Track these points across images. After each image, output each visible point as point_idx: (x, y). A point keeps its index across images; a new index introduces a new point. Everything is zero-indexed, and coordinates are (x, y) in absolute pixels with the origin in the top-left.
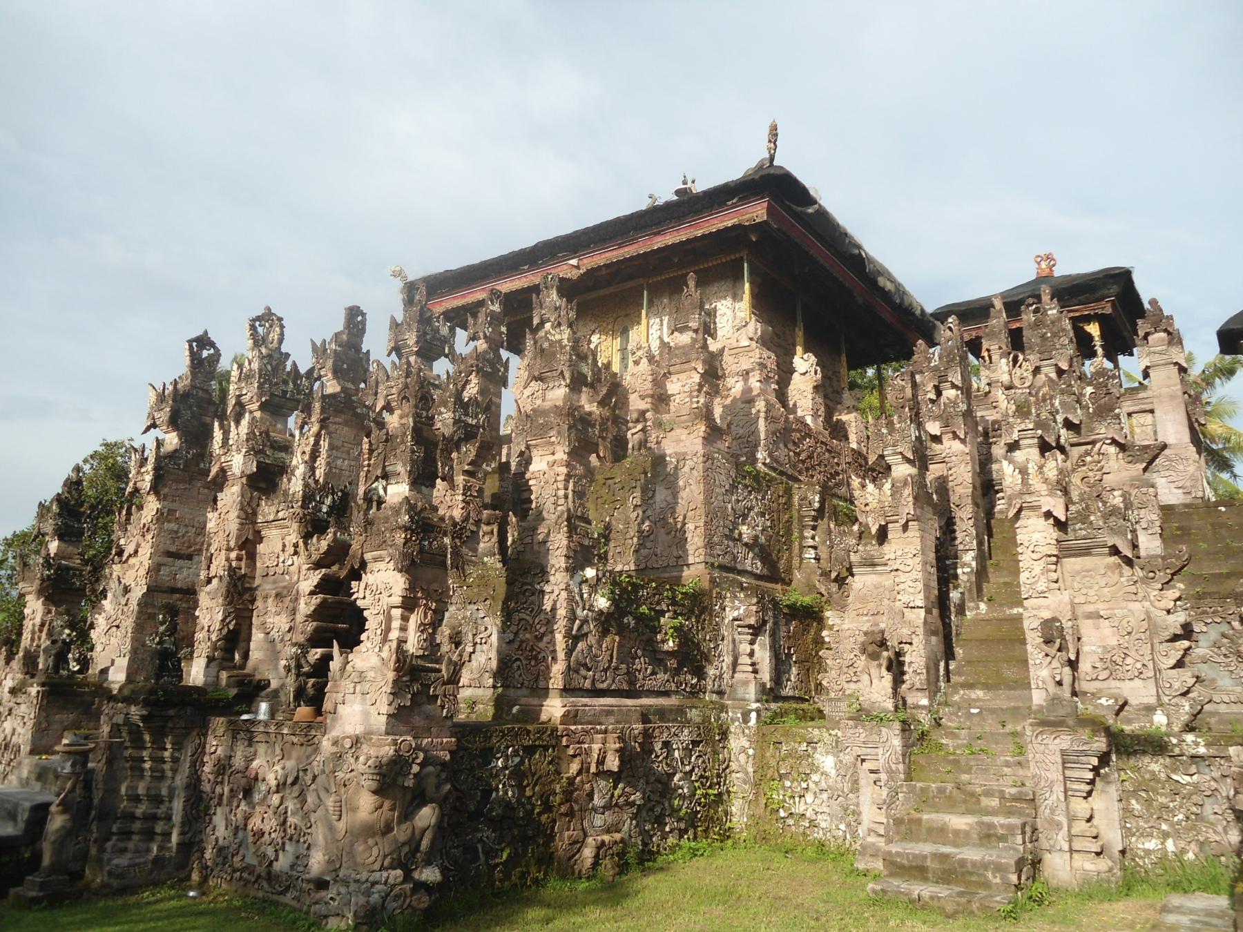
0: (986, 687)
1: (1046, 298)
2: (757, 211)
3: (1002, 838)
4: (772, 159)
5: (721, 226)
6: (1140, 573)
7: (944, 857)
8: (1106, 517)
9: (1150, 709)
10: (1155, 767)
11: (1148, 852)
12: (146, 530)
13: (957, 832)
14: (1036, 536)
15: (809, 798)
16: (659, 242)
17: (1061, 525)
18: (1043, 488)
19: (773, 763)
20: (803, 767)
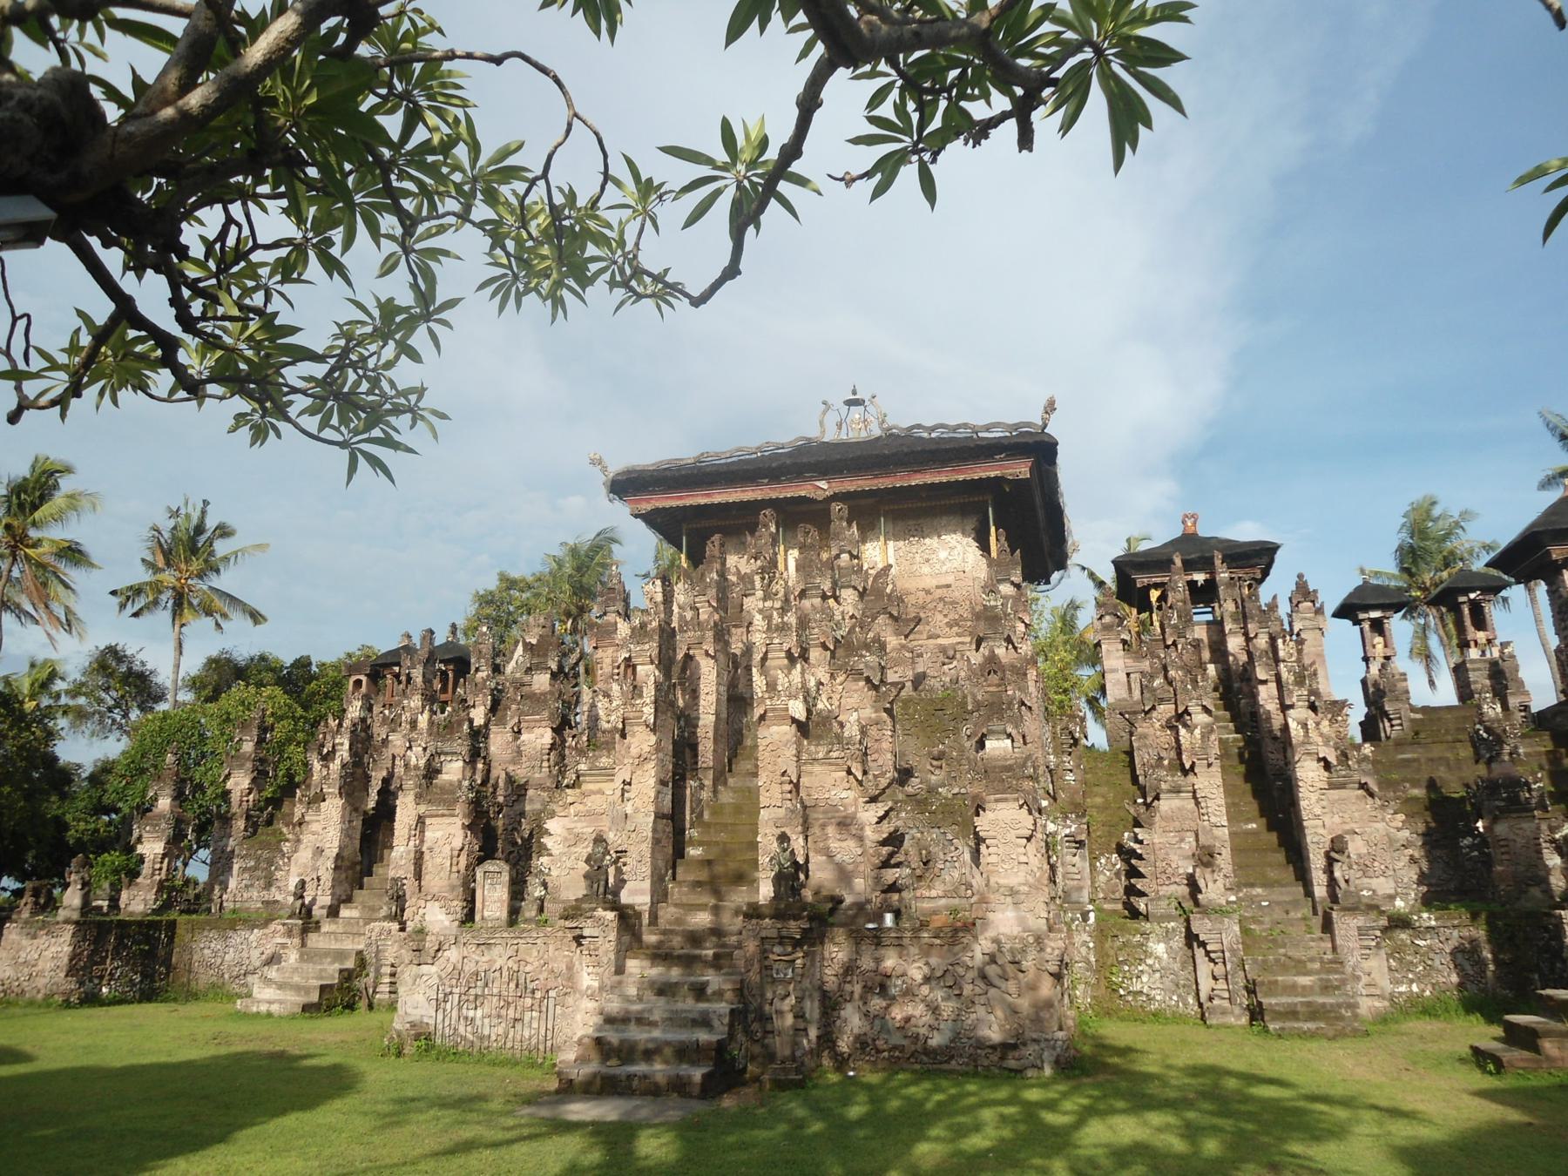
0: (1263, 886)
1: (1218, 562)
2: (1021, 469)
3: (1337, 988)
4: (1045, 426)
5: (984, 475)
6: (1379, 802)
7: (1309, 1004)
8: (1359, 762)
9: (1392, 898)
10: (1403, 936)
11: (1401, 993)
12: (642, 760)
13: (1304, 987)
14: (1311, 774)
15: (1145, 978)
16: (917, 480)
17: (1327, 766)
18: (1319, 740)
19: (1112, 952)
20: (1140, 954)
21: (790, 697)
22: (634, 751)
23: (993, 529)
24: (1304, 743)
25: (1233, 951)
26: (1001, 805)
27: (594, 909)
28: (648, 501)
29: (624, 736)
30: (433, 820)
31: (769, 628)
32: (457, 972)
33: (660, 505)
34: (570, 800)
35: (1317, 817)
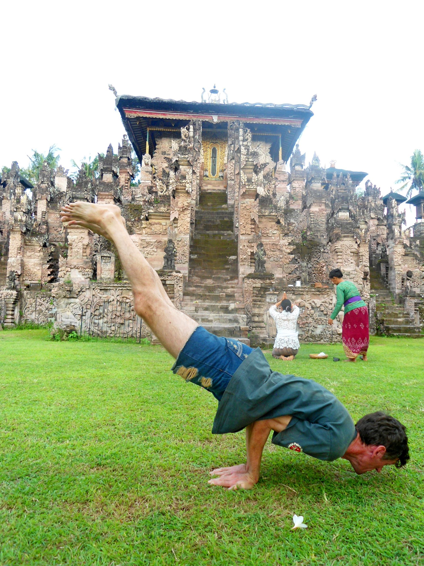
3: (411, 322)
6: (418, 262)
8: (415, 246)
13: (400, 322)
18: (404, 237)
21: (258, 185)
22: (180, 205)
23: (281, 148)
24: (399, 238)
25: (373, 310)
26: (345, 239)
27: (171, 272)
28: (135, 112)
29: (174, 197)
30: (72, 230)
31: (247, 154)
32: (89, 304)
33: (141, 115)
34: (144, 226)
35: (400, 265)
